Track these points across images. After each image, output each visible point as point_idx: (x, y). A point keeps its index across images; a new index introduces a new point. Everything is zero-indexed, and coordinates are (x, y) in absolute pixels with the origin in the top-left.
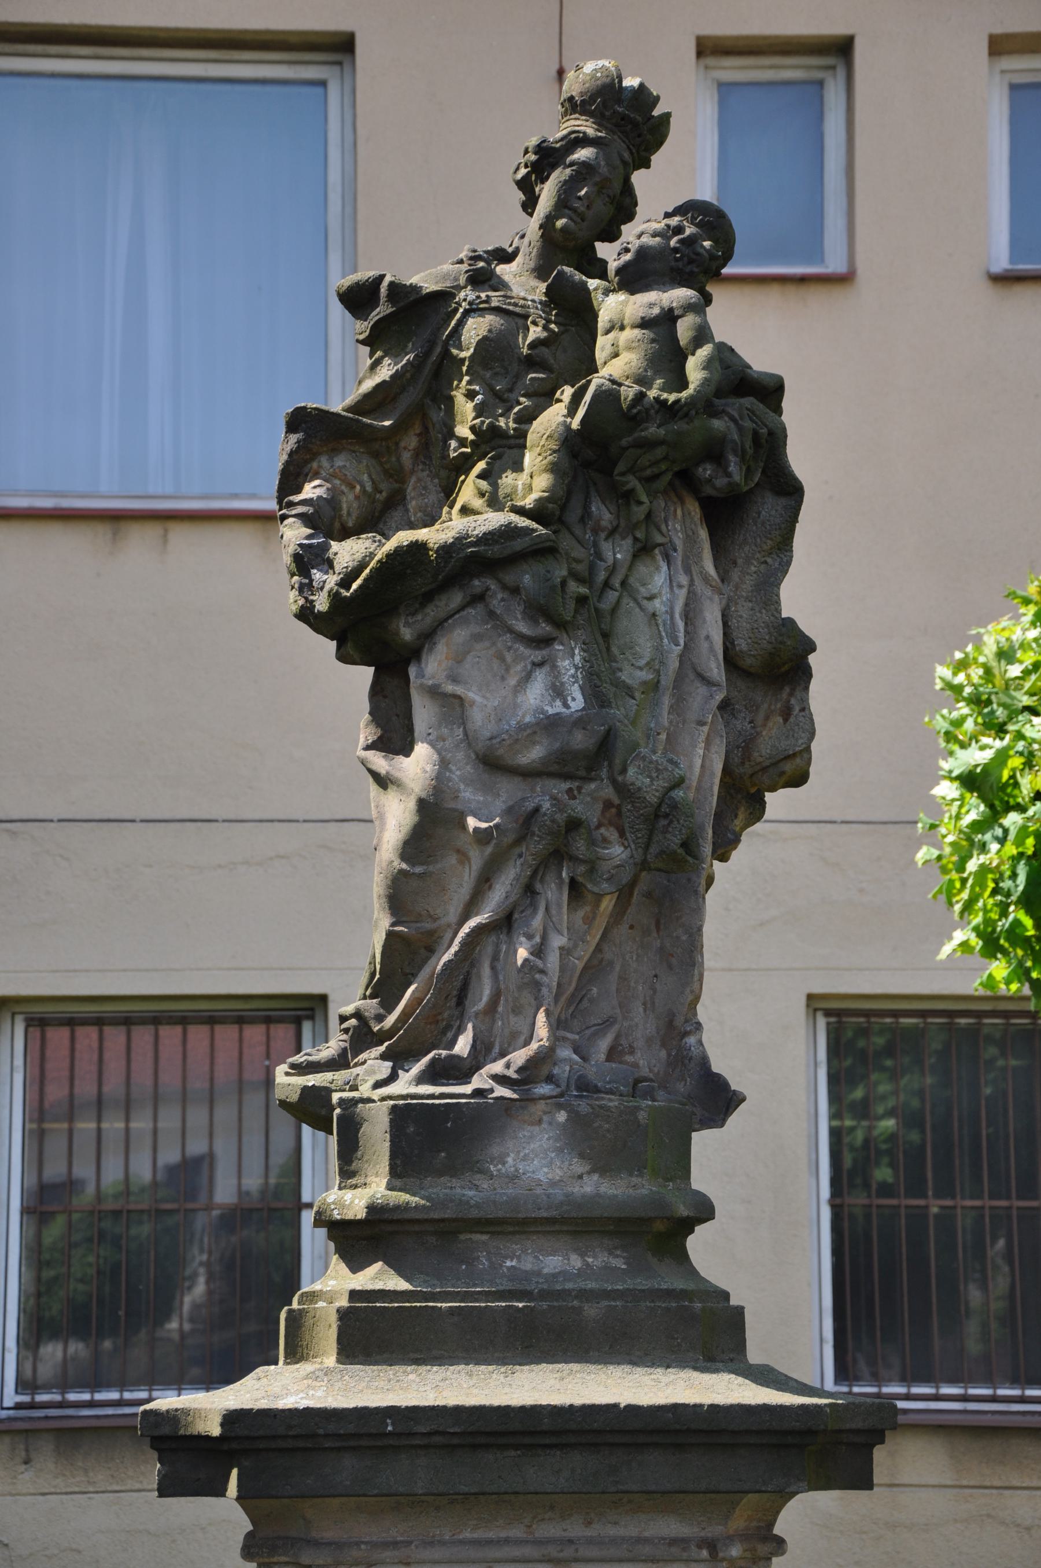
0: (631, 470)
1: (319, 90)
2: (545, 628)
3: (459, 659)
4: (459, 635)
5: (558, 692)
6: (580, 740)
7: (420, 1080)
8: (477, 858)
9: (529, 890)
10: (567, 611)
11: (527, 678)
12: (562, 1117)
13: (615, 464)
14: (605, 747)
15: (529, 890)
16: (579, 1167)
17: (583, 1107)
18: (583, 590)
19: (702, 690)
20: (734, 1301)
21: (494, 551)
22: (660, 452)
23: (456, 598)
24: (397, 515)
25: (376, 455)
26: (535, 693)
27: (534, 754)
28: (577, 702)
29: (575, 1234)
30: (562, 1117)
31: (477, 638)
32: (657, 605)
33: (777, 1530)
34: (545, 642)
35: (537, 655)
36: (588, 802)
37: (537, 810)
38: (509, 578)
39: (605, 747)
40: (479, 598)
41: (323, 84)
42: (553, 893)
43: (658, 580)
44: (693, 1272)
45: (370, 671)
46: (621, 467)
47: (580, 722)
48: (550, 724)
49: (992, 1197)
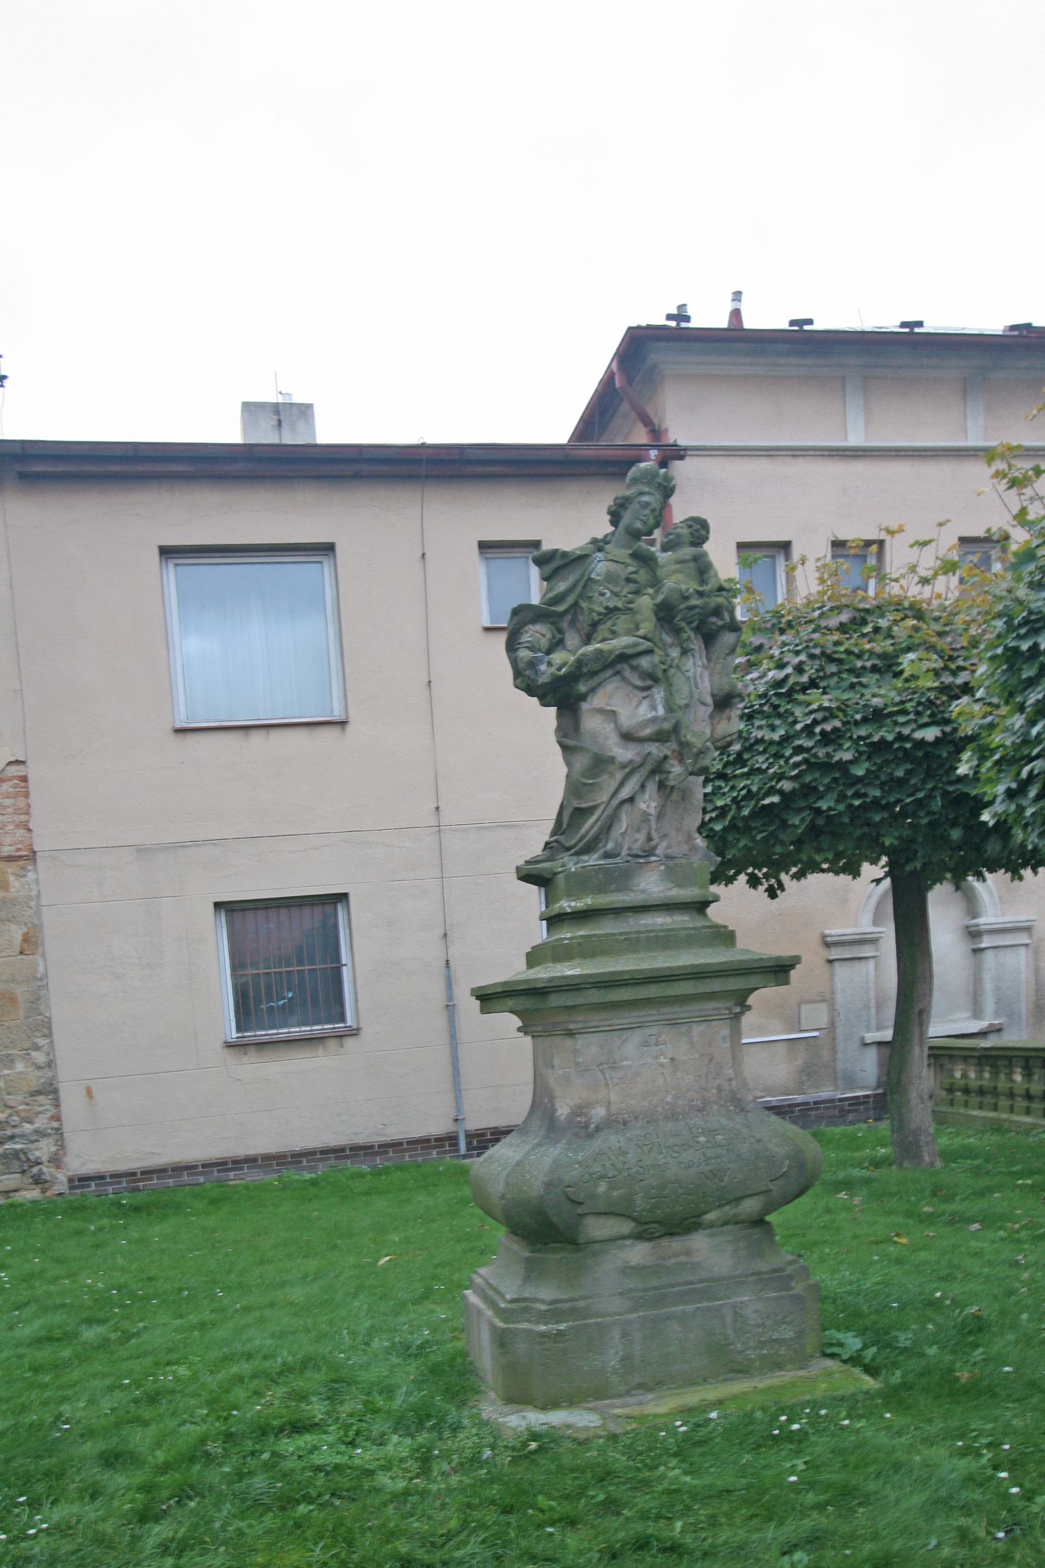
0: (683, 619)
1: (319, 565)
2: (649, 683)
3: (610, 697)
4: (609, 687)
5: (654, 708)
6: (667, 726)
7: (599, 859)
8: (619, 776)
9: (643, 786)
10: (660, 674)
11: (639, 704)
12: (662, 868)
13: (674, 617)
14: (676, 729)
15: (643, 786)
16: (670, 885)
17: (671, 863)
18: (665, 667)
19: (702, 708)
20: (730, 928)
21: (629, 651)
22: (697, 611)
23: (610, 672)
24: (561, 646)
25: (552, 623)
26: (639, 711)
27: (647, 732)
28: (661, 711)
29: (668, 910)
30: (662, 868)
31: (617, 688)
32: (690, 674)
33: (748, 1003)
34: (648, 688)
35: (645, 694)
36: (666, 749)
37: (649, 753)
38: (635, 662)
39: (676, 729)
40: (618, 673)
41: (321, 562)
42: (652, 787)
43: (689, 663)
44: (709, 920)
45: (555, 708)
46: (678, 618)
47: (665, 719)
48: (654, 720)
49: (280, 973)
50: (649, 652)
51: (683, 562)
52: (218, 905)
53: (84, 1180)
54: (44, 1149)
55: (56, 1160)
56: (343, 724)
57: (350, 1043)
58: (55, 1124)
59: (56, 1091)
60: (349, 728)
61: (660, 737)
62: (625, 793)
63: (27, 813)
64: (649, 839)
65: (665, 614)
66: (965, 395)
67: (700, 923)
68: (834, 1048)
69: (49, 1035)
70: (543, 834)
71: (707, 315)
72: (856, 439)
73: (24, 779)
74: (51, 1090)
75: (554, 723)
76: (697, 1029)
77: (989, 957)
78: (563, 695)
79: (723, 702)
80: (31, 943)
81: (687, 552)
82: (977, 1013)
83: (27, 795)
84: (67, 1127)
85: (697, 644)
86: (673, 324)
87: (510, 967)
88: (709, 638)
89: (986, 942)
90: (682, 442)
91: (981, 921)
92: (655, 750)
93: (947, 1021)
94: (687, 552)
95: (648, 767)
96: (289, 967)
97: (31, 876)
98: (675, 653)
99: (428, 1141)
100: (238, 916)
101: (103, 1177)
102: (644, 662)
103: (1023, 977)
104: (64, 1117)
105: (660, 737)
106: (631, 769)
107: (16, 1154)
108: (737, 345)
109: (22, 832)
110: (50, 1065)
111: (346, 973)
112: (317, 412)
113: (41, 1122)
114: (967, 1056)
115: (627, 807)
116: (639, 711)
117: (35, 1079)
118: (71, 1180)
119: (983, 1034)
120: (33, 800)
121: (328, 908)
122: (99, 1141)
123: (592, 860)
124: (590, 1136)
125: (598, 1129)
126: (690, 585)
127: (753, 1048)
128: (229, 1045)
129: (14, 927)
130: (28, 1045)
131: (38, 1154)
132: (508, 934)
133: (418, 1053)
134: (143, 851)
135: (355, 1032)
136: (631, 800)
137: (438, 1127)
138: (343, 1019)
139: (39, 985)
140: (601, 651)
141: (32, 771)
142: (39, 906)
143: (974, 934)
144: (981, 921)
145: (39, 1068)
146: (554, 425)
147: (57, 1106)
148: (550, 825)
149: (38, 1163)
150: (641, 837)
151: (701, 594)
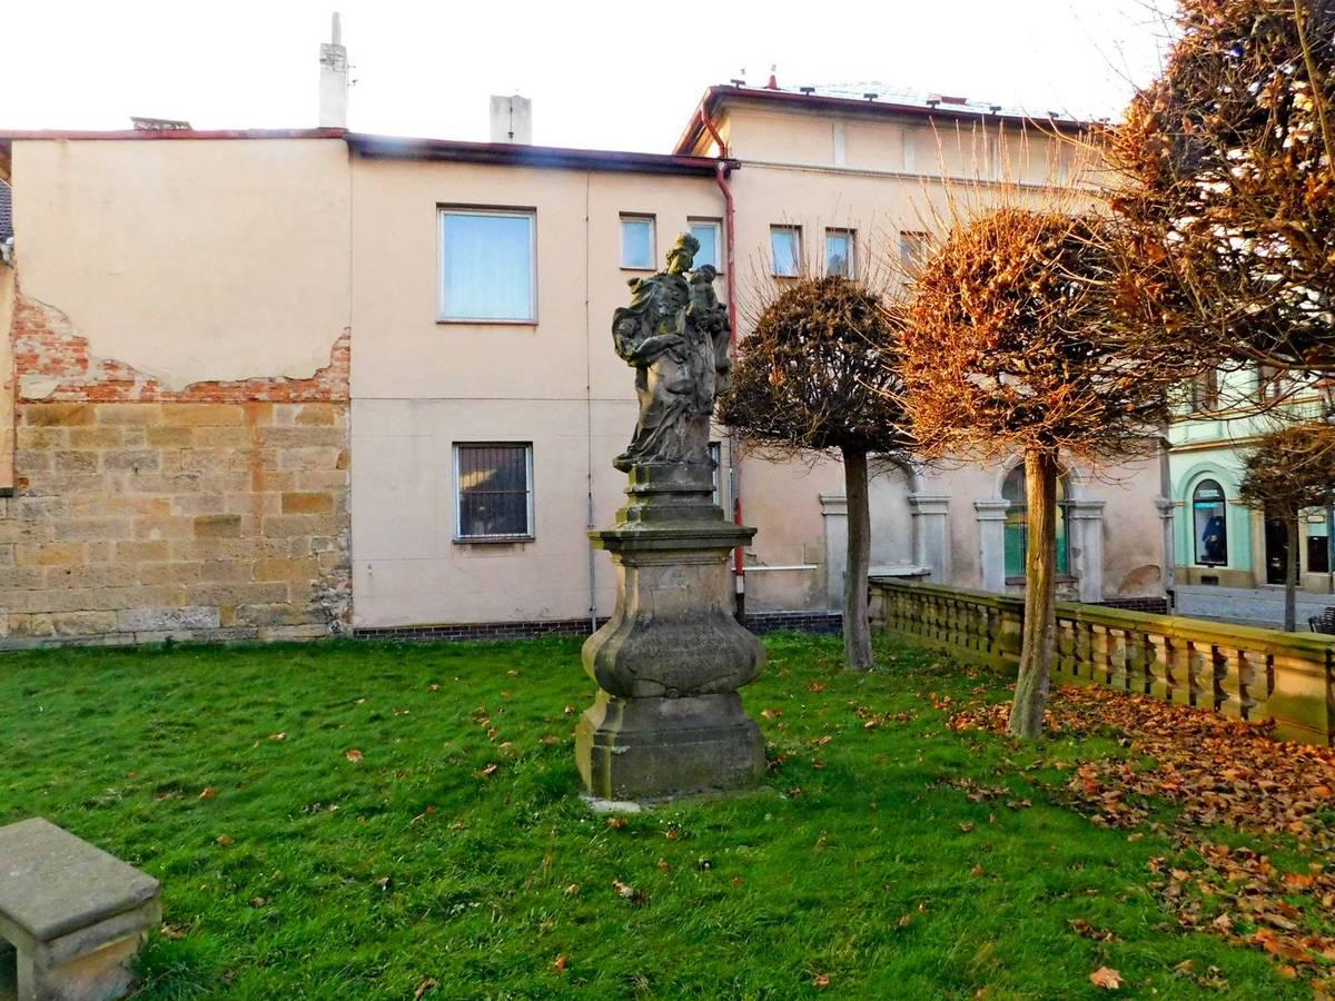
26: (678, 375)
27: (680, 388)
42: (682, 420)
48: (684, 381)
50: (682, 343)
51: (700, 292)
52: (454, 443)
53: (364, 632)
54: (341, 608)
55: (347, 617)
56: (535, 325)
57: (528, 547)
58: (348, 591)
59: (350, 568)
60: (538, 328)
61: (686, 393)
62: (669, 423)
63: (348, 372)
64: (679, 451)
65: (691, 320)
66: (903, 145)
67: (705, 503)
68: (826, 580)
69: (349, 527)
70: (628, 442)
71: (756, 82)
72: (840, 163)
73: (348, 349)
74: (347, 566)
75: (635, 377)
76: (703, 569)
77: (922, 519)
78: (641, 362)
79: (723, 370)
80: (343, 461)
81: (703, 286)
82: (915, 562)
83: (349, 360)
84: (356, 593)
85: (708, 337)
86: (734, 85)
87: (608, 523)
88: (715, 335)
89: (921, 508)
90: (739, 158)
91: (916, 494)
92: (682, 398)
93: (888, 563)
94: (703, 286)
95: (680, 409)
96: (496, 498)
97: (347, 415)
98: (696, 343)
99: (573, 624)
100: (466, 451)
101: (374, 632)
102: (678, 348)
103: (943, 537)
104: (354, 584)
105: (686, 393)
106: (673, 409)
107: (325, 609)
108: (771, 100)
109: (343, 385)
110: (349, 547)
111: (529, 497)
112: (534, 107)
113: (341, 588)
114: (905, 591)
115: (669, 431)
116: (678, 375)
117: (338, 558)
118: (355, 632)
119: (912, 577)
120: (352, 364)
121: (520, 451)
122: (377, 604)
123: (651, 461)
124: (643, 631)
125: (648, 626)
126: (703, 307)
127: (776, 575)
128: (455, 543)
129: (334, 450)
130: (336, 533)
131: (336, 611)
132: (615, 495)
133: (553, 572)
134: (413, 401)
135: (532, 540)
136: (672, 426)
137: (579, 612)
138: (525, 530)
139: (345, 488)
140: (654, 342)
141: (353, 344)
142: (350, 436)
143: (913, 503)
144: (916, 494)
145: (342, 550)
146: (666, 143)
147: (350, 577)
148: (631, 438)
149: (336, 618)
150: (675, 449)
151: (709, 312)
